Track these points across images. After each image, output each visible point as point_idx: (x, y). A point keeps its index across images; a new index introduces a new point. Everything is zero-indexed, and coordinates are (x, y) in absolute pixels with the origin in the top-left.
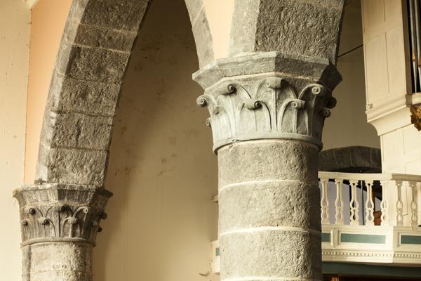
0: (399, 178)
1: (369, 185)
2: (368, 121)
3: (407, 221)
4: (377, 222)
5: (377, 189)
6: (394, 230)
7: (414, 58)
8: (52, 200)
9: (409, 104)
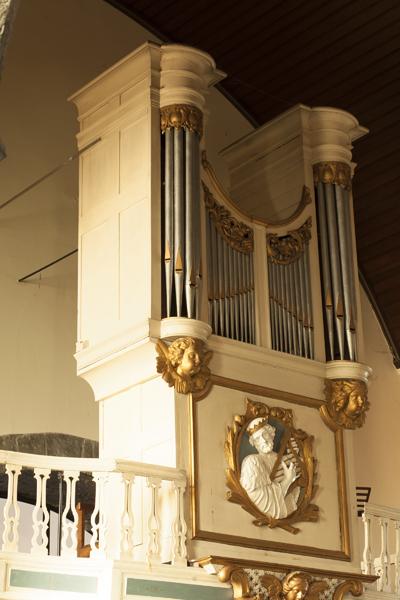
0: (129, 470)
1: (71, 479)
2: (78, 373)
3: (140, 555)
4: (83, 550)
5: (86, 489)
6: (115, 568)
7: (167, 256)
8: (256, 579)
9: (153, 336)
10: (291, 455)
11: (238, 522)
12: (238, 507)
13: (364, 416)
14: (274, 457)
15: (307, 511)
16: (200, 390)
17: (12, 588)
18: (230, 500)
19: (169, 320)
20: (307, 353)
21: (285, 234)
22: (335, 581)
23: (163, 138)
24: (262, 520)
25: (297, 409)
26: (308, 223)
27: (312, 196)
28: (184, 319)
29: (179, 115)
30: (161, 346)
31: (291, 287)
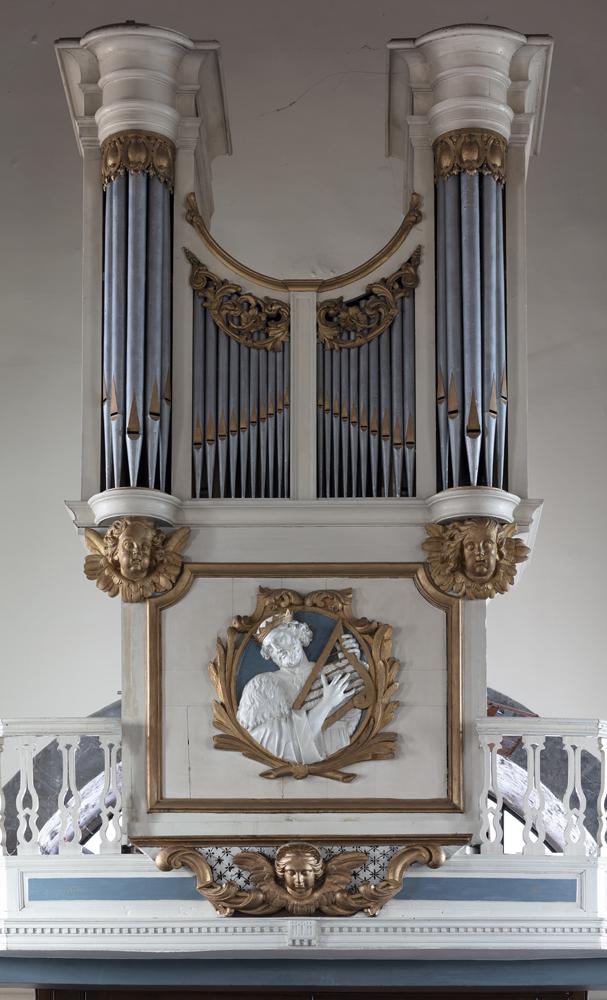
10: (345, 662)
11: (239, 776)
12: (236, 757)
14: (306, 669)
18: (216, 747)
19: (446, 493)
20: (407, 489)
23: (104, 194)
24: (282, 770)
27: (427, 208)
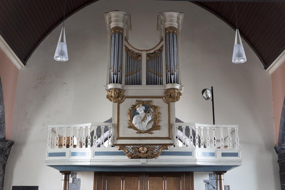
1: (184, 128)
10: (151, 113)
11: (132, 133)
13: (110, 100)
14: (144, 114)
15: (156, 127)
16: (120, 101)
17: (72, 157)
21: (154, 52)
22: (158, 146)
24: (140, 132)
25: (154, 100)
26: (162, 47)
28: (114, 84)
29: (113, 30)
30: (108, 92)
31: (156, 66)
